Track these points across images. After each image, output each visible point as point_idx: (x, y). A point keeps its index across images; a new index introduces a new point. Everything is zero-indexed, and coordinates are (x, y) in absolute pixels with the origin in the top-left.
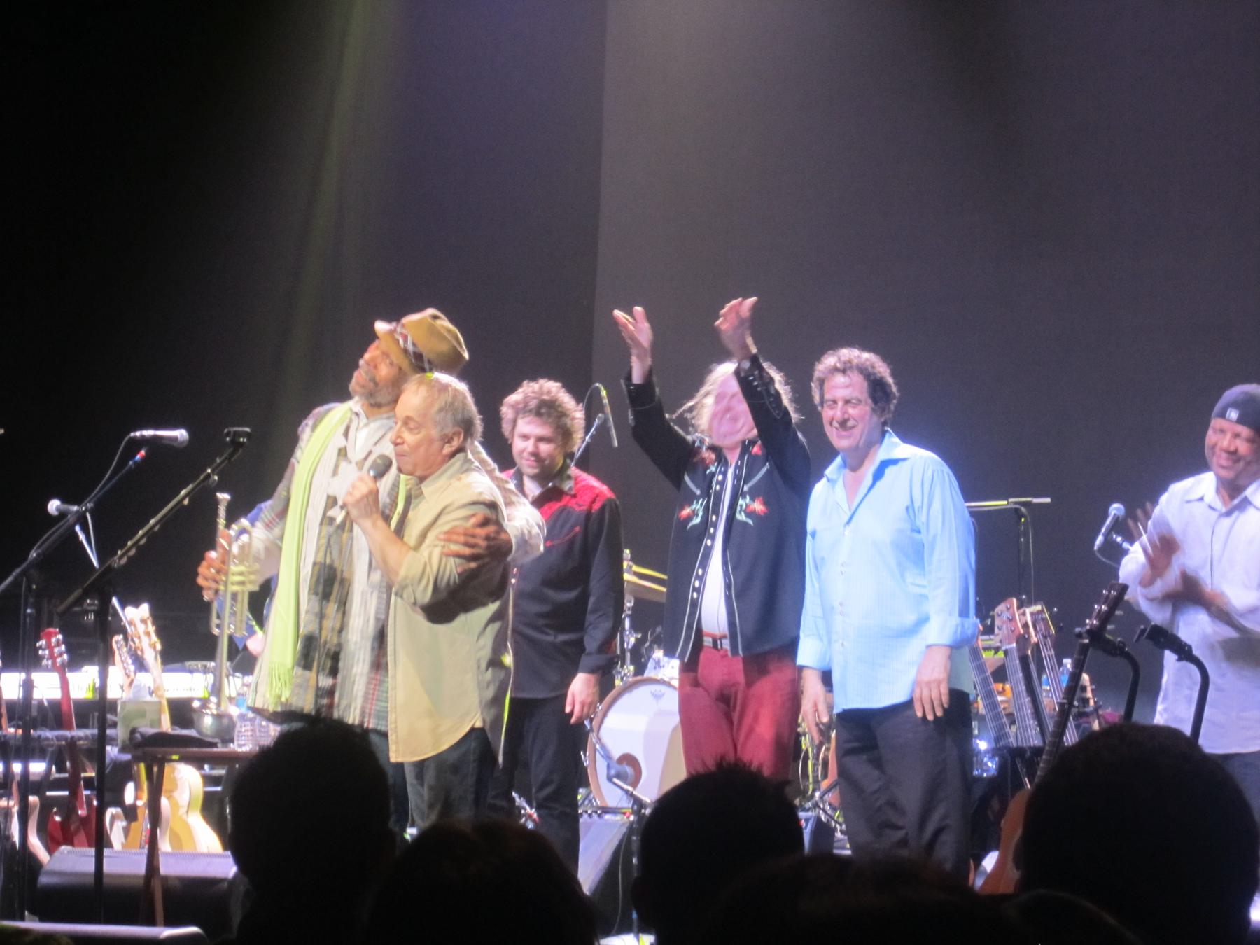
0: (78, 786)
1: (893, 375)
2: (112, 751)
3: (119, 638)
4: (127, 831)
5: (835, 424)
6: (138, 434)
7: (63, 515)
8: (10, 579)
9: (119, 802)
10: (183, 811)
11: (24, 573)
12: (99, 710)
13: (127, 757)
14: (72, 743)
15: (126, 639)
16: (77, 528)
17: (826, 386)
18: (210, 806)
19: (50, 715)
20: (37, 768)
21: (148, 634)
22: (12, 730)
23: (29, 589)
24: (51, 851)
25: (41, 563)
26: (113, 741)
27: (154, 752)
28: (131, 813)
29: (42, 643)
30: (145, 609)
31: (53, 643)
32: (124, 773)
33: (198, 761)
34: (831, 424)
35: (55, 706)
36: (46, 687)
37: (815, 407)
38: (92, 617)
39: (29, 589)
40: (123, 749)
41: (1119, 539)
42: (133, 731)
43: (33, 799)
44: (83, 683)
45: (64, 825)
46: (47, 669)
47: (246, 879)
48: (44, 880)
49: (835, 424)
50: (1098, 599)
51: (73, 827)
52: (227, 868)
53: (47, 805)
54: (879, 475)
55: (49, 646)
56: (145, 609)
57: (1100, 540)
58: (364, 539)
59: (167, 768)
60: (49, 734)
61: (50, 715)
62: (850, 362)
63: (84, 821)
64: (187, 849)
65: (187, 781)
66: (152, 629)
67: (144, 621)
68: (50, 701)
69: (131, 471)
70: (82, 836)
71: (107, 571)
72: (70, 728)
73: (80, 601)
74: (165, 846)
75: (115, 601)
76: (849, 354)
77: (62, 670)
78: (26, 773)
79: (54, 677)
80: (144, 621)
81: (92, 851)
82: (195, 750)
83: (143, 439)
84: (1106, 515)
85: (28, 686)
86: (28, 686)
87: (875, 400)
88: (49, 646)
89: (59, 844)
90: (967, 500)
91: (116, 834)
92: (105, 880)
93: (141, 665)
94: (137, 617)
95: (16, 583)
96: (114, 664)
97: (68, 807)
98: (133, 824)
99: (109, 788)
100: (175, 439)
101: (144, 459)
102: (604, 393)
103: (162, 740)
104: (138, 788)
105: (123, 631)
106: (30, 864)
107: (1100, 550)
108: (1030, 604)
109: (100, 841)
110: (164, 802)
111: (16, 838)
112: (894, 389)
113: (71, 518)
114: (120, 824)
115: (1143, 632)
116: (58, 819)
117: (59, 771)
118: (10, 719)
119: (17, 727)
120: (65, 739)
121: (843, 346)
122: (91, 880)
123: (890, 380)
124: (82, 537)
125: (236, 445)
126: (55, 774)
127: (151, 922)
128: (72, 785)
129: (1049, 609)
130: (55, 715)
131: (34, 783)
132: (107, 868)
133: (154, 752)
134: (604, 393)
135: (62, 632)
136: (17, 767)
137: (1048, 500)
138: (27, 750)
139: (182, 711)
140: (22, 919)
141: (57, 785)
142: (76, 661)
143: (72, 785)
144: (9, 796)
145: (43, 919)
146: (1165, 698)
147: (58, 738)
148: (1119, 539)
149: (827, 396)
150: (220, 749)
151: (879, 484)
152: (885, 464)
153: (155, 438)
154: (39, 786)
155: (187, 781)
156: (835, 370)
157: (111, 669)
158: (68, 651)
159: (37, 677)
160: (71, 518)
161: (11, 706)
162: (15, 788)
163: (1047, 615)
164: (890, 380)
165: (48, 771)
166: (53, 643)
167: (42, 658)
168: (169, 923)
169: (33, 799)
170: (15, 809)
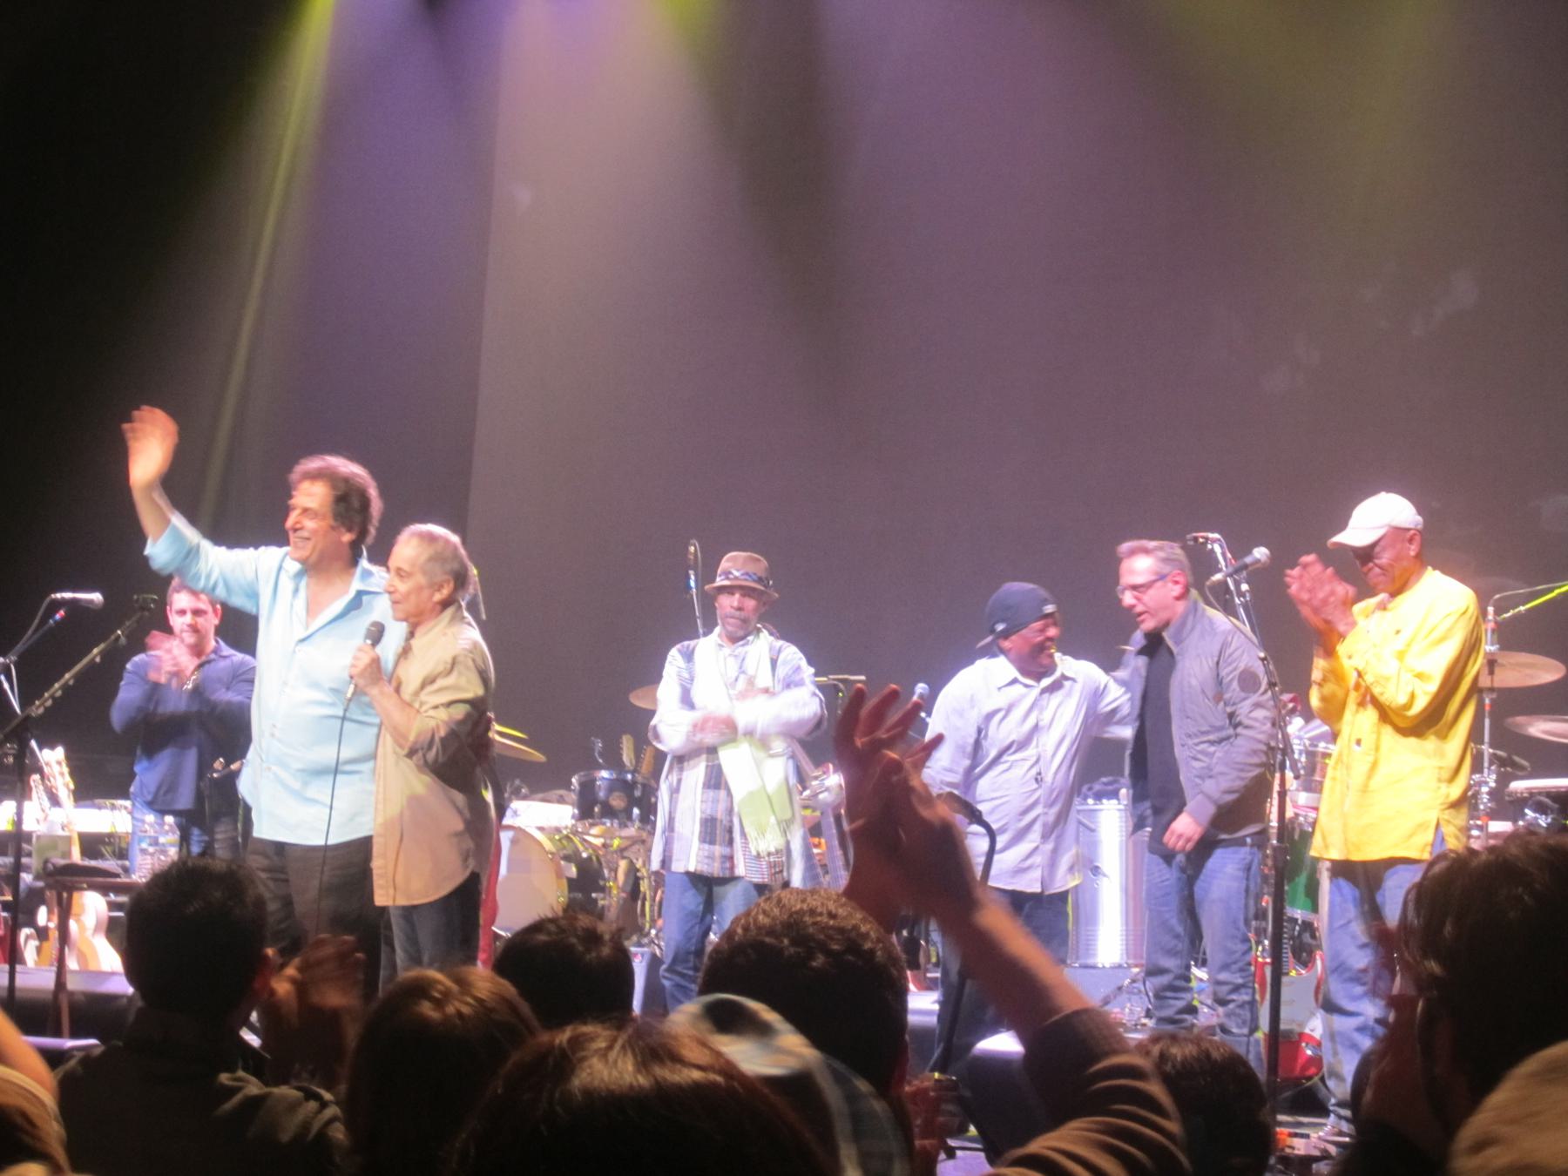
1: (382, 521)
2: (27, 878)
3: (36, 777)
4: (39, 950)
6: (59, 596)
9: (32, 923)
10: (89, 932)
13: (40, 884)
21: (62, 774)
26: (27, 869)
27: (64, 882)
28: (42, 934)
30: (59, 752)
32: (36, 897)
33: (104, 890)
38: (11, 759)
40: (37, 878)
42: (46, 862)
56: (59, 752)
65: (92, 907)
66: (66, 770)
69: (51, 629)
74: (72, 964)
75: (33, 743)
80: (59, 763)
92: (18, 994)
93: (55, 801)
94: (53, 758)
98: (46, 945)
100: (91, 601)
101: (63, 619)
104: (50, 912)
105: (40, 771)
114: (33, 943)
124: (6, 686)
127: (57, 1033)
133: (64, 882)
139: (92, 845)
150: (124, 879)
153: (74, 601)
155: (92, 907)
157: (27, 804)
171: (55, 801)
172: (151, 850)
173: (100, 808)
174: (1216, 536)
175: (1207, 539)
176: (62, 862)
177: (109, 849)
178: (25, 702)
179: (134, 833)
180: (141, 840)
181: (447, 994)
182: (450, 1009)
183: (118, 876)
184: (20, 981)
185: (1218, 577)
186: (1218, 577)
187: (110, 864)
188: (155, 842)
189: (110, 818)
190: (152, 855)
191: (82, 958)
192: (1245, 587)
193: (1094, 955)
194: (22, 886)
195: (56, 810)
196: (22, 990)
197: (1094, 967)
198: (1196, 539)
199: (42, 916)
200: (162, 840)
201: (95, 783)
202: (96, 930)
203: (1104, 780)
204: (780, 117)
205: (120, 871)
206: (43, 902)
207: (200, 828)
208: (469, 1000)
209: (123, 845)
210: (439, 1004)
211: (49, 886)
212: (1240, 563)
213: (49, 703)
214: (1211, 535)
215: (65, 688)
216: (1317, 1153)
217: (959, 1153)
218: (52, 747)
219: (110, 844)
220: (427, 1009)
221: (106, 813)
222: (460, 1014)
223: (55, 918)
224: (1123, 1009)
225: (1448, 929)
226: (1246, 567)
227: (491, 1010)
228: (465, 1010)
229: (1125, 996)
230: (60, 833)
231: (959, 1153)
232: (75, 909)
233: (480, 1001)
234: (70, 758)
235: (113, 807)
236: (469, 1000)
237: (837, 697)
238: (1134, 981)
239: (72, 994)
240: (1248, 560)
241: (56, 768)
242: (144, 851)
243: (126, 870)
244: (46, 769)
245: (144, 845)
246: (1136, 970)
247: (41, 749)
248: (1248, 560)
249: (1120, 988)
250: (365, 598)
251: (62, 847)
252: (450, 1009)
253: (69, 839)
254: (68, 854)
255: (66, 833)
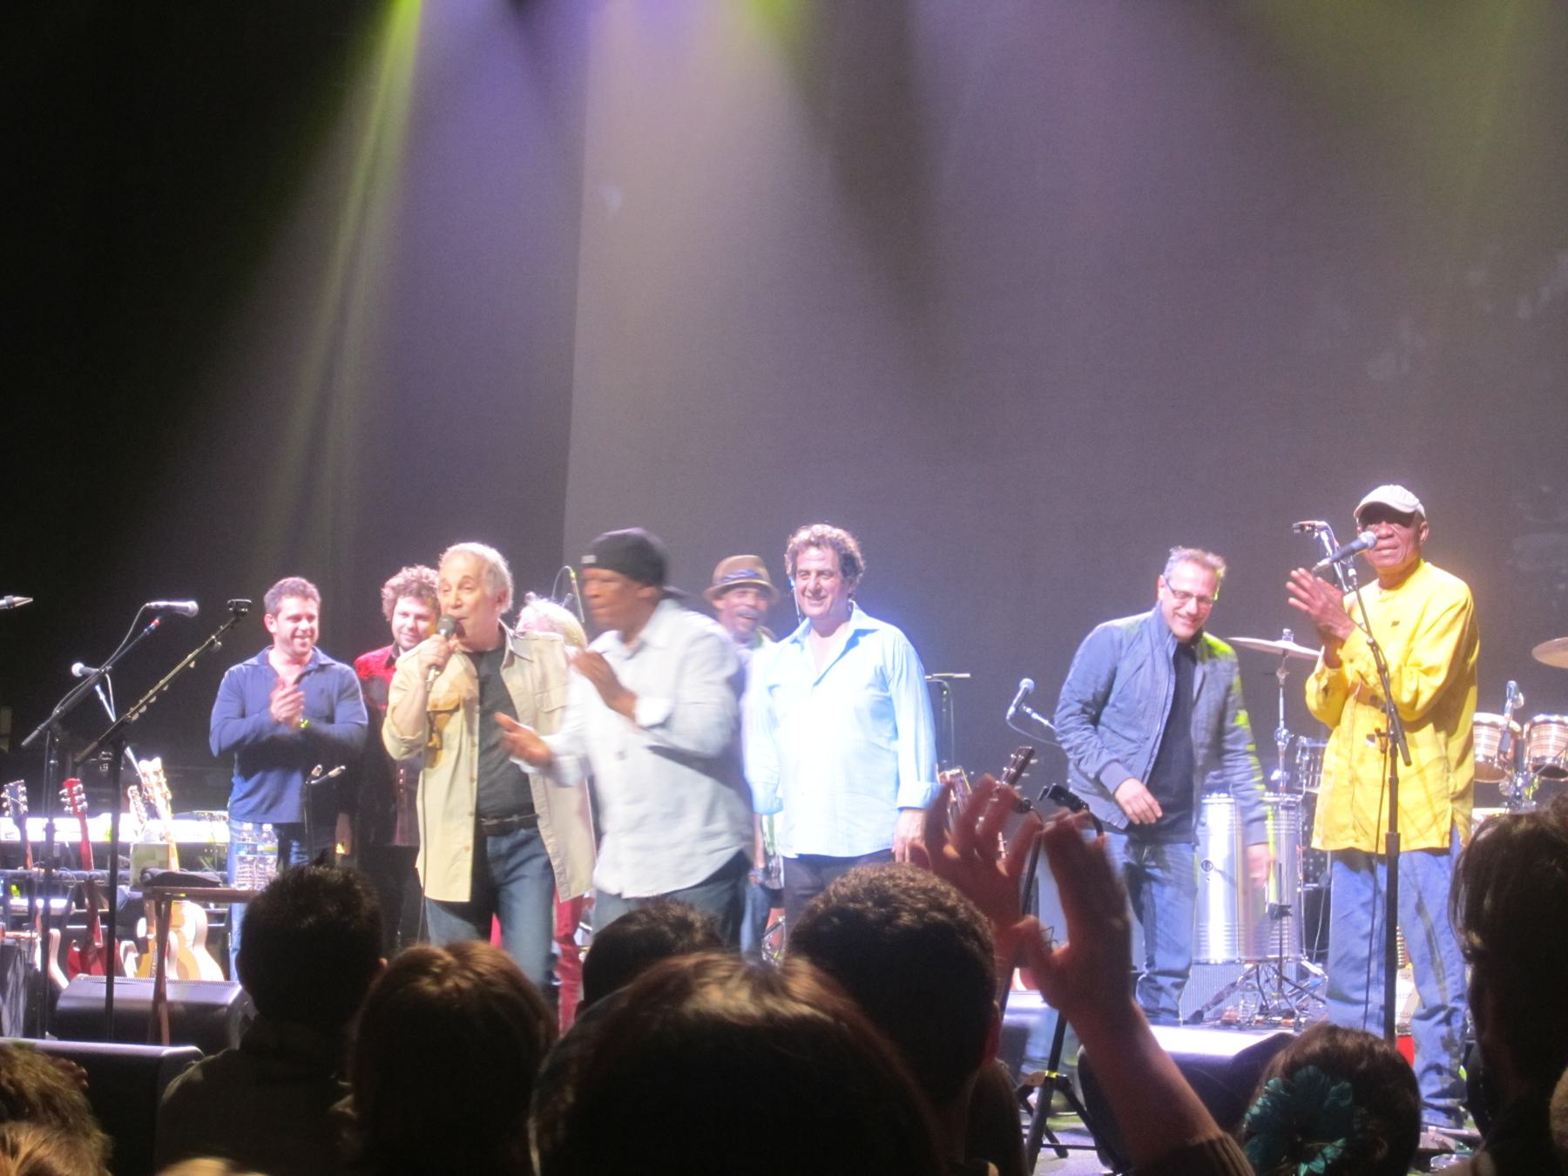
0: (94, 919)
1: (862, 551)
2: (124, 890)
3: (133, 788)
4: (138, 961)
5: (808, 594)
6: (153, 604)
7: (85, 676)
8: (35, 733)
9: (131, 935)
10: (189, 944)
11: (48, 727)
12: (111, 854)
13: (139, 895)
14: (90, 882)
15: (140, 789)
16: (98, 688)
17: (799, 558)
18: (215, 940)
19: (73, 858)
20: (58, 904)
21: (160, 784)
22: (36, 869)
23: (52, 740)
24: (69, 977)
25: (65, 719)
26: (125, 880)
27: (162, 890)
28: (142, 946)
29: (65, 791)
30: (157, 763)
31: (75, 792)
32: (135, 910)
33: (202, 899)
34: (803, 593)
35: (75, 847)
36: (67, 831)
37: (786, 576)
38: (106, 767)
39: (52, 740)
40: (135, 888)
41: (1029, 710)
42: (144, 872)
43: (55, 932)
44: (99, 829)
45: (82, 955)
46: (68, 815)
47: (250, 997)
48: (62, 1004)
49: (808, 594)
50: (1007, 762)
51: (90, 957)
52: (234, 992)
53: (66, 939)
54: (852, 643)
55: (71, 795)
56: (157, 763)
57: (1012, 710)
58: (394, 697)
59: (174, 906)
60: (69, 873)
61: (73, 858)
62: (823, 537)
63: (99, 951)
64: (193, 977)
65: (191, 917)
66: (163, 780)
67: (156, 773)
68: (71, 845)
69: (146, 637)
70: (98, 965)
71: (122, 724)
72: (88, 868)
73: (95, 753)
74: (171, 974)
75: (129, 752)
76: (819, 529)
77: (82, 816)
78: (47, 909)
79: (75, 823)
80: (156, 773)
81: (104, 978)
82: (203, 892)
83: (158, 611)
84: (1018, 689)
85: (50, 830)
86: (50, 830)
87: (845, 573)
88: (71, 795)
89: (77, 972)
90: (927, 673)
91: (129, 964)
92: (116, 1005)
93: (153, 812)
94: (151, 770)
95: (41, 737)
96: (127, 810)
97: (86, 939)
98: (145, 956)
99: (120, 922)
100: (186, 609)
101: (158, 627)
102: (573, 575)
103: (170, 879)
104: (149, 924)
105: (138, 783)
106: (53, 991)
107: (1012, 718)
108: (950, 767)
109: (112, 968)
110: (172, 937)
111: (39, 967)
112: (862, 563)
113: (92, 680)
114: (133, 956)
115: (1046, 791)
116: (77, 949)
117: (78, 907)
118: (35, 860)
119: (41, 866)
120: (84, 877)
121: (816, 522)
122: (103, 1004)
123: (858, 555)
124: (102, 697)
125: (237, 613)
126: (74, 910)
127: (157, 1041)
128: (89, 919)
129: (967, 772)
130: (75, 856)
131: (56, 917)
132: (117, 993)
133: (162, 890)
134: (573, 575)
135: (83, 782)
136: (40, 903)
137: (967, 675)
138: (50, 887)
139: (190, 855)
140: (43, 1037)
141: (76, 919)
142: (93, 811)
143: (89, 919)
144: (32, 928)
145: (61, 1038)
146: (1402, 930)
147: (78, 877)
148: (1029, 710)
149: (801, 566)
150: (222, 888)
151: (852, 651)
152: (860, 633)
153: (169, 608)
154: (60, 920)
155: (191, 917)
156: (809, 544)
157: (123, 816)
158: (88, 799)
159: (58, 822)
160: (92, 680)
161: (36, 847)
162: (38, 921)
163: (965, 777)
164: (858, 555)
165: (69, 907)
166: (75, 792)
167: (64, 804)
168: (173, 1043)
169: (55, 932)
170: (39, 940)
171: (153, 812)
172: (250, 857)
173: (198, 819)
174: (1323, 523)
175: (1313, 527)
176: (161, 871)
177: (209, 860)
178: (121, 709)
179: (232, 843)
180: (239, 849)
181: (446, 968)
182: (449, 984)
183: (216, 884)
184: (118, 992)
185: (1325, 562)
186: (1325, 562)
187: (210, 874)
188: (254, 851)
189: (210, 829)
190: (251, 863)
191: (182, 969)
192: (1352, 572)
193: (1207, 952)
194: (119, 899)
195: (155, 821)
196: (122, 1001)
197: (1207, 964)
198: (1302, 527)
199: (142, 928)
200: (260, 848)
201: (192, 793)
202: (196, 941)
203: (1214, 773)
204: (871, 106)
205: (218, 880)
206: (142, 914)
207: (298, 840)
208: (470, 975)
209: (223, 856)
210: (439, 979)
211: (147, 897)
212: (1346, 548)
213: (144, 709)
214: (1317, 523)
215: (159, 693)
216: (1435, 1147)
217: (1070, 1151)
218: (150, 758)
219: (208, 855)
220: (428, 985)
221: (205, 824)
222: (457, 988)
223: (154, 930)
224: (1237, 1006)
225: (1487, 902)
226: (1353, 552)
227: (489, 983)
228: (464, 984)
229: (1238, 993)
230: (158, 842)
231: (1070, 1151)
232: (174, 921)
233: (479, 975)
234: (168, 769)
235: (212, 818)
236: (470, 975)
237: (941, 695)
238: (1247, 978)
239: (171, 1004)
240: (1355, 545)
241: (154, 779)
242: (242, 859)
243: (226, 881)
244: (144, 780)
245: (242, 853)
246: (1248, 966)
247: (138, 760)
248: (1355, 545)
249: (1233, 985)
250: (861, 639)
251: (160, 857)
252: (449, 984)
253: (167, 848)
254: (166, 863)
255: (164, 842)
